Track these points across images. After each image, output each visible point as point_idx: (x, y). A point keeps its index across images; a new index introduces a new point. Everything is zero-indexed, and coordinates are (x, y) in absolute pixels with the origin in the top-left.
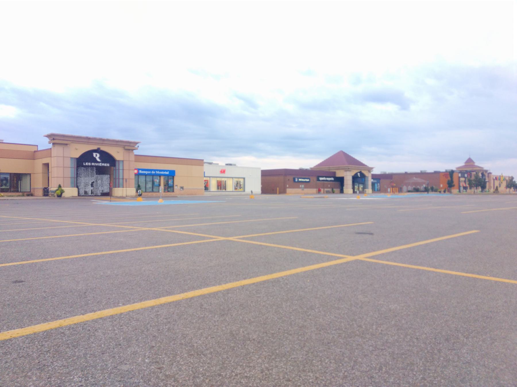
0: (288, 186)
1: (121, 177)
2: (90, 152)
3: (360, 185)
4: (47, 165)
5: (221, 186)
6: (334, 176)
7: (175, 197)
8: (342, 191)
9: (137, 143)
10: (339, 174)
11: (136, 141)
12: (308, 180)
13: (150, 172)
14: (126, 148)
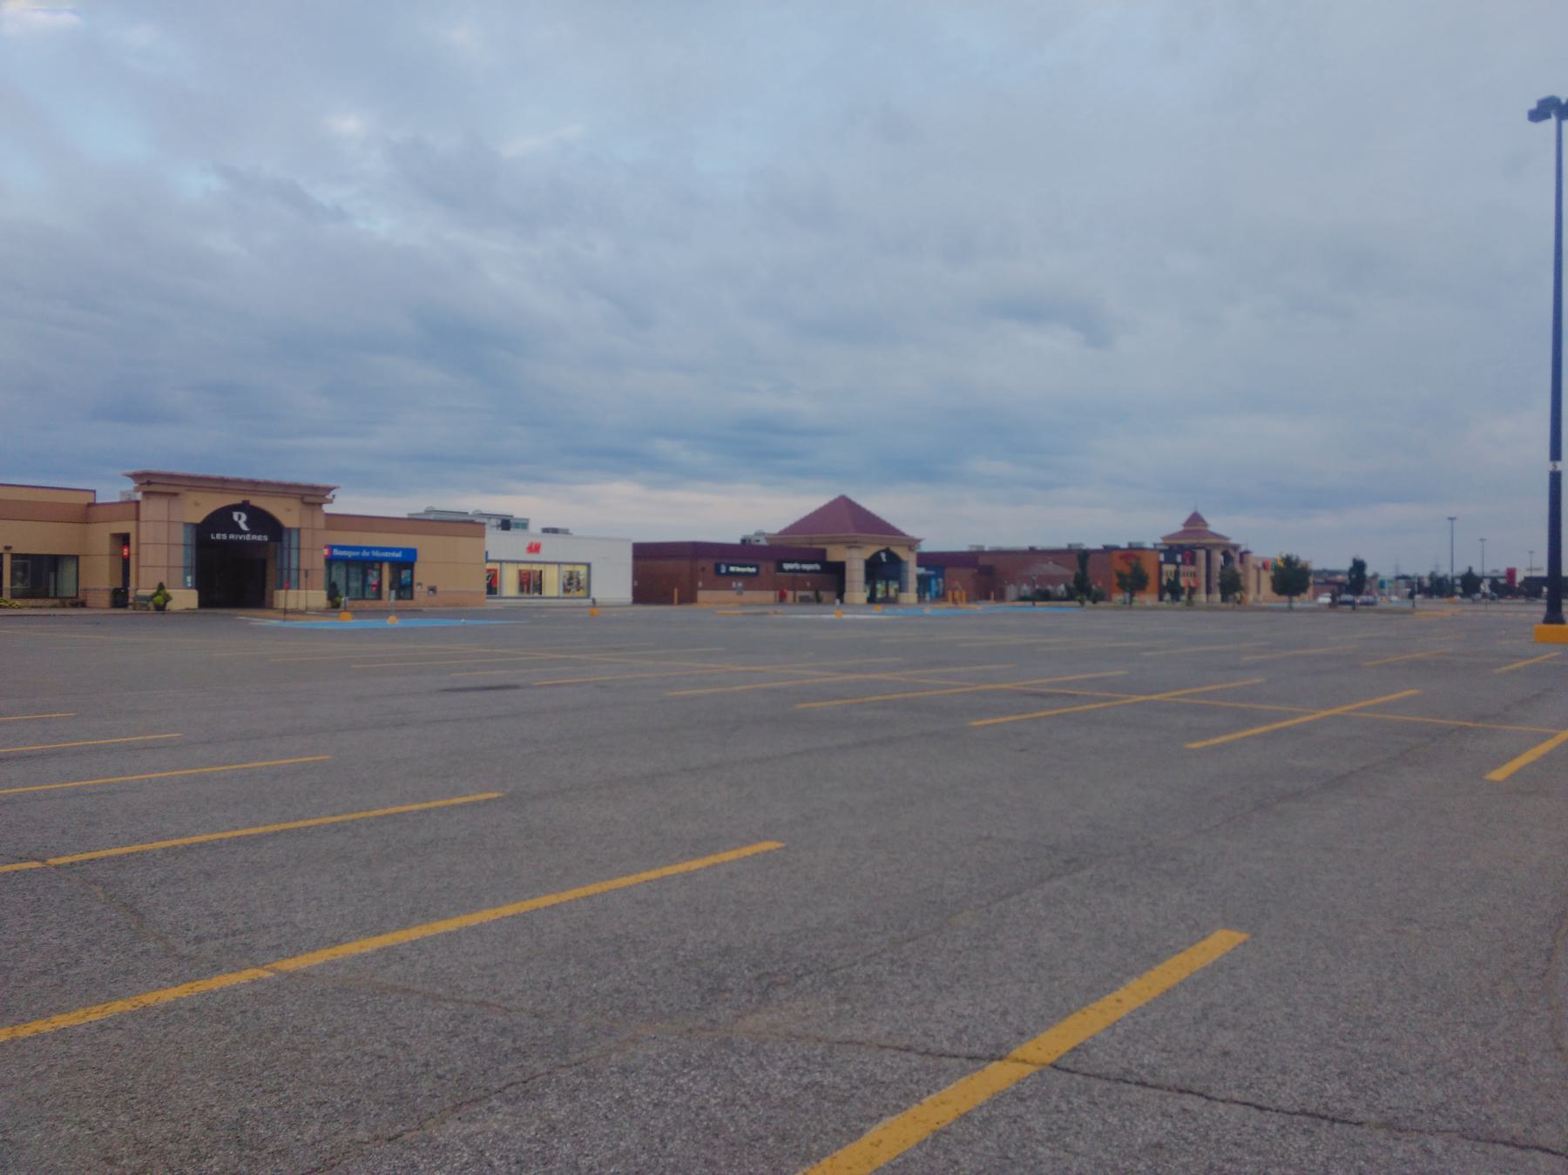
1: (294, 564)
2: (227, 511)
4: (124, 539)
5: (530, 583)
7: (415, 612)
8: (840, 594)
9: (330, 489)
10: (835, 554)
11: (330, 484)
12: (753, 570)
13: (356, 554)
14: (309, 499)
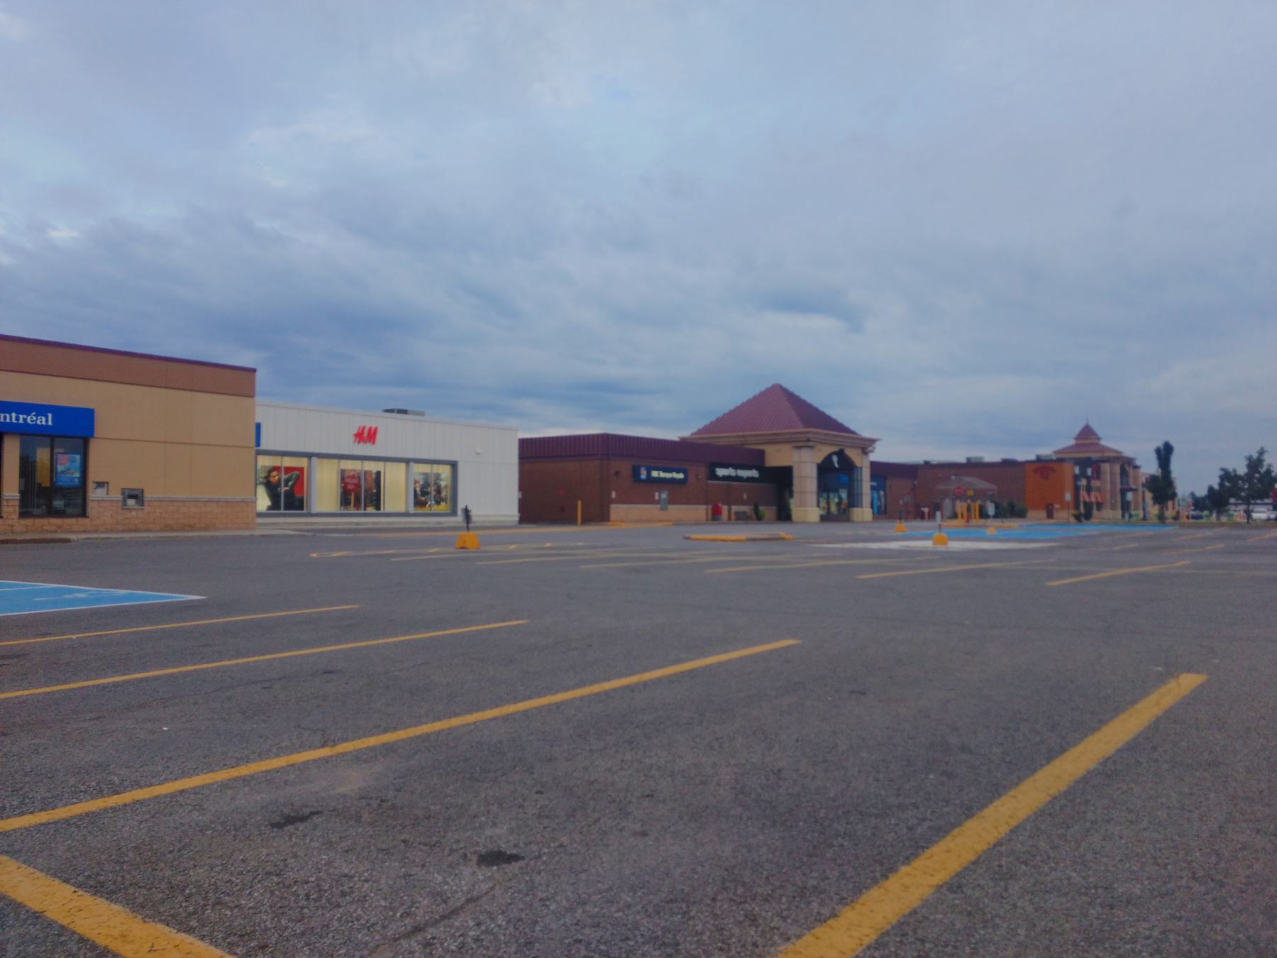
0: (614, 495)
3: (831, 495)
5: (360, 493)
6: (756, 463)
8: (784, 515)
10: (777, 457)
12: (681, 476)
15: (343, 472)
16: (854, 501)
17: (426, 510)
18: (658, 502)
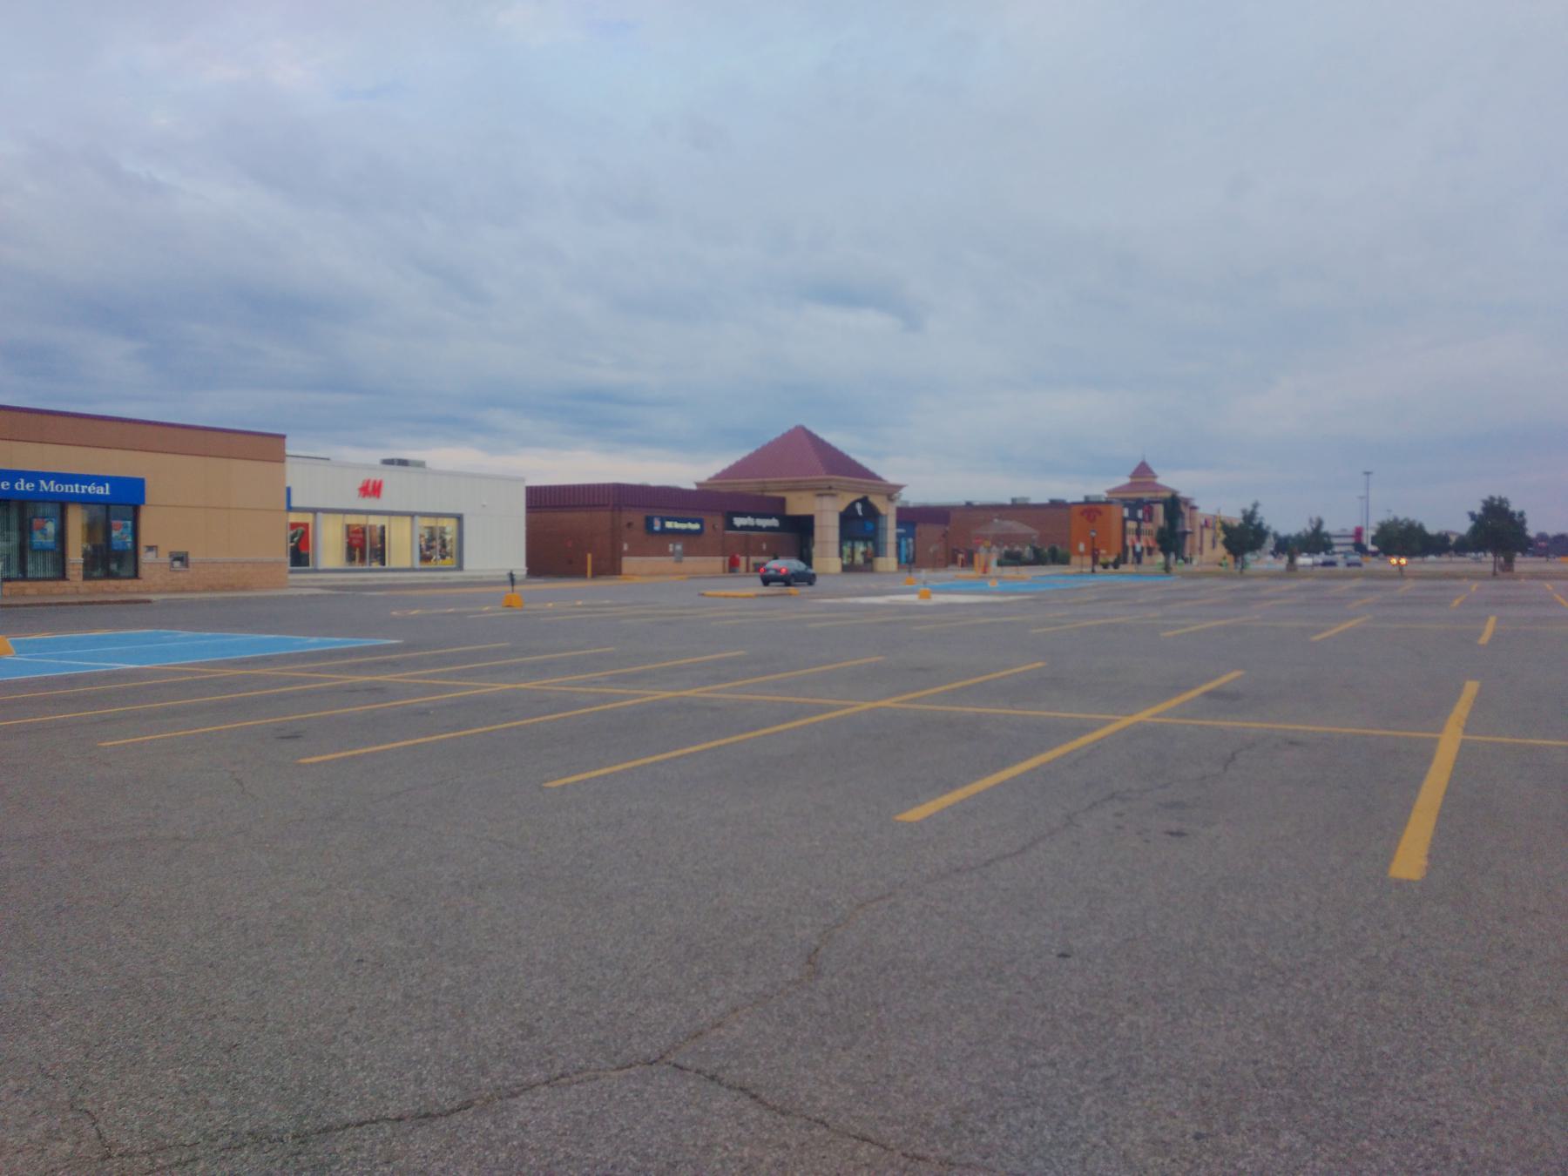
0: (626, 547)
5: (364, 546)
6: (779, 514)
10: (798, 505)
12: (696, 526)
15: (348, 527)
16: (878, 551)
17: (431, 565)
18: (672, 554)
